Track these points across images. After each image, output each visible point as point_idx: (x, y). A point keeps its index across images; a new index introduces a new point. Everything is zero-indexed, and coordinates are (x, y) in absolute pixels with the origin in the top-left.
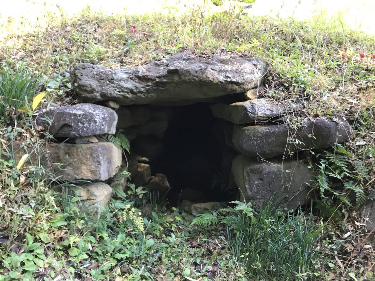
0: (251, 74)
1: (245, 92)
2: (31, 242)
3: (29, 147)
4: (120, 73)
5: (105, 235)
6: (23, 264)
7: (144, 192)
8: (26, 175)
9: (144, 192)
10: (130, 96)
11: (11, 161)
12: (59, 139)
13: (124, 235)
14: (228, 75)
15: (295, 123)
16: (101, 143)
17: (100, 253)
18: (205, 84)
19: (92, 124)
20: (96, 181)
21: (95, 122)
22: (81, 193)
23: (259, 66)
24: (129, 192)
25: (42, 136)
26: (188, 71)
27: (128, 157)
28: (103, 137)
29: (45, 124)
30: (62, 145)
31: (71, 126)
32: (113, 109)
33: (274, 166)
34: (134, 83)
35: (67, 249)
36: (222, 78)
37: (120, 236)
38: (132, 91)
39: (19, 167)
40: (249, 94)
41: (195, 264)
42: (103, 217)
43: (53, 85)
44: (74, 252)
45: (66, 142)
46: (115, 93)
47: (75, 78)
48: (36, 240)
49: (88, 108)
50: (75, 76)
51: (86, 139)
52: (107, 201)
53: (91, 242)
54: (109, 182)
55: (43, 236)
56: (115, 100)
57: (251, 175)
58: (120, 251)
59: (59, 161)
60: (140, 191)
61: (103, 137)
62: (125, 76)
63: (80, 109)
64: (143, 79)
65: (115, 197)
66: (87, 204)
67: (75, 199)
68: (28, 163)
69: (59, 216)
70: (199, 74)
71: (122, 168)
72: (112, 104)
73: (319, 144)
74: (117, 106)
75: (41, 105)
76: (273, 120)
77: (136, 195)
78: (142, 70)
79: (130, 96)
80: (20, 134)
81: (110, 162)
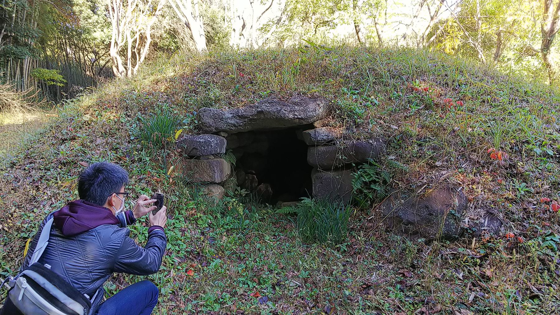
0: (318, 109)
1: (545, 31)
2: (177, 214)
3: (175, 162)
4: (227, 112)
5: (219, 216)
6: (174, 224)
7: (246, 192)
8: (173, 178)
9: (246, 192)
10: (233, 128)
11: (164, 170)
12: (191, 157)
13: (231, 218)
14: (296, 113)
15: (340, 144)
16: (215, 159)
17: (215, 224)
18: (282, 120)
19: (210, 147)
20: (213, 183)
21: (212, 146)
22: (204, 190)
23: (321, 105)
24: (236, 193)
25: (181, 155)
26: (269, 112)
27: (235, 169)
28: (217, 155)
29: (182, 148)
30: (192, 160)
31: (197, 149)
32: (224, 137)
33: (331, 174)
34: (236, 120)
35: (196, 220)
36: (291, 116)
37: (228, 218)
38: (235, 126)
39: (168, 174)
40: (316, 124)
41: (274, 235)
42: (218, 205)
43: (187, 121)
44: (200, 222)
45: (195, 159)
46: (223, 126)
47: (199, 118)
48: (179, 214)
49: (207, 137)
50: (200, 116)
51: (206, 156)
52: (221, 197)
53: (210, 219)
54: (222, 184)
55: (183, 212)
56: (224, 131)
57: (316, 180)
58: (227, 225)
59: (191, 170)
60: (244, 192)
61: (217, 155)
62: (230, 116)
63: (202, 138)
64: (242, 117)
65: (227, 195)
66: (208, 197)
67: (200, 193)
68: (173, 171)
69: (191, 202)
70: (276, 114)
71: (231, 175)
72: (222, 134)
73: (358, 158)
74: (226, 135)
75: (180, 136)
76: (330, 142)
77: (241, 195)
78: (242, 110)
79: (233, 128)
80: (168, 154)
81: (222, 171)
